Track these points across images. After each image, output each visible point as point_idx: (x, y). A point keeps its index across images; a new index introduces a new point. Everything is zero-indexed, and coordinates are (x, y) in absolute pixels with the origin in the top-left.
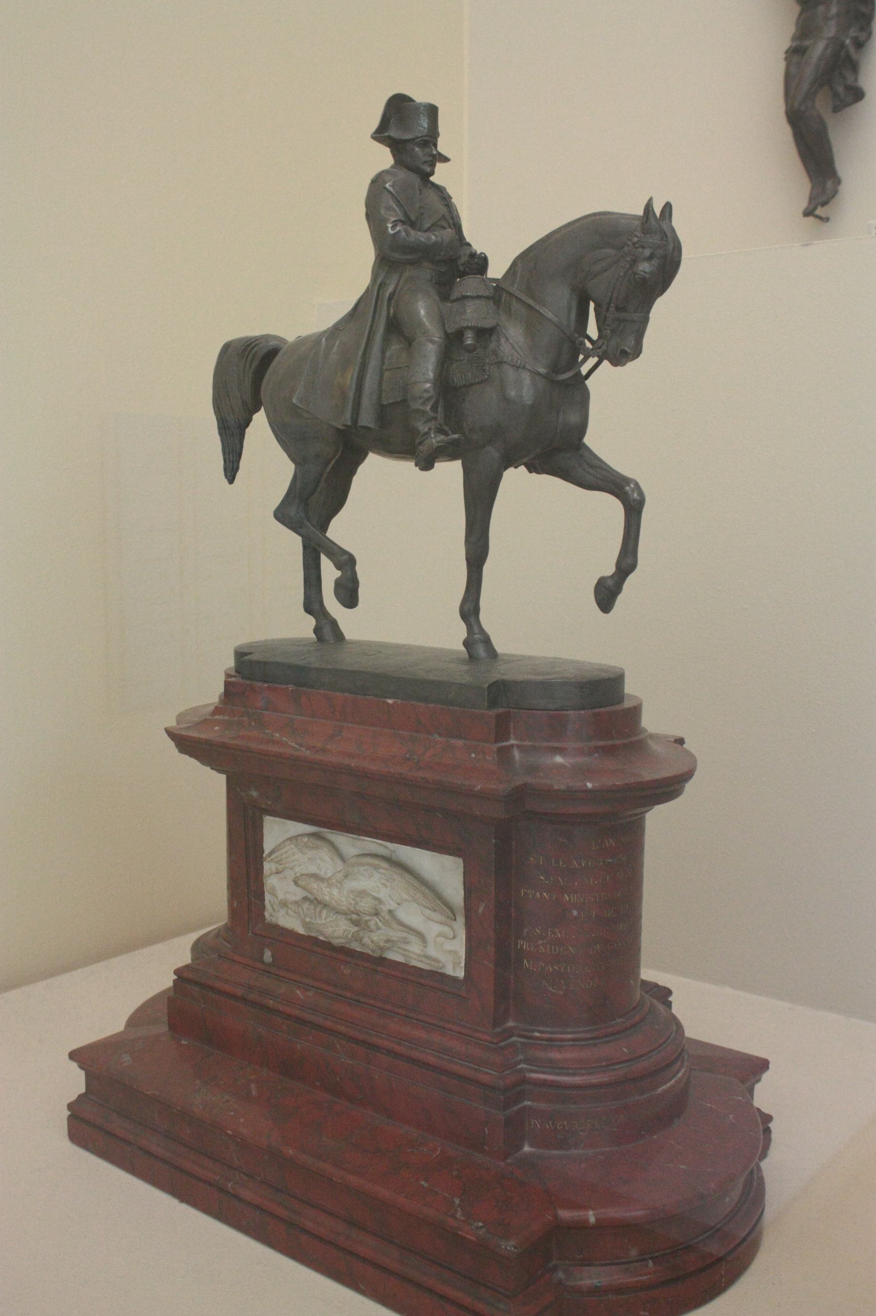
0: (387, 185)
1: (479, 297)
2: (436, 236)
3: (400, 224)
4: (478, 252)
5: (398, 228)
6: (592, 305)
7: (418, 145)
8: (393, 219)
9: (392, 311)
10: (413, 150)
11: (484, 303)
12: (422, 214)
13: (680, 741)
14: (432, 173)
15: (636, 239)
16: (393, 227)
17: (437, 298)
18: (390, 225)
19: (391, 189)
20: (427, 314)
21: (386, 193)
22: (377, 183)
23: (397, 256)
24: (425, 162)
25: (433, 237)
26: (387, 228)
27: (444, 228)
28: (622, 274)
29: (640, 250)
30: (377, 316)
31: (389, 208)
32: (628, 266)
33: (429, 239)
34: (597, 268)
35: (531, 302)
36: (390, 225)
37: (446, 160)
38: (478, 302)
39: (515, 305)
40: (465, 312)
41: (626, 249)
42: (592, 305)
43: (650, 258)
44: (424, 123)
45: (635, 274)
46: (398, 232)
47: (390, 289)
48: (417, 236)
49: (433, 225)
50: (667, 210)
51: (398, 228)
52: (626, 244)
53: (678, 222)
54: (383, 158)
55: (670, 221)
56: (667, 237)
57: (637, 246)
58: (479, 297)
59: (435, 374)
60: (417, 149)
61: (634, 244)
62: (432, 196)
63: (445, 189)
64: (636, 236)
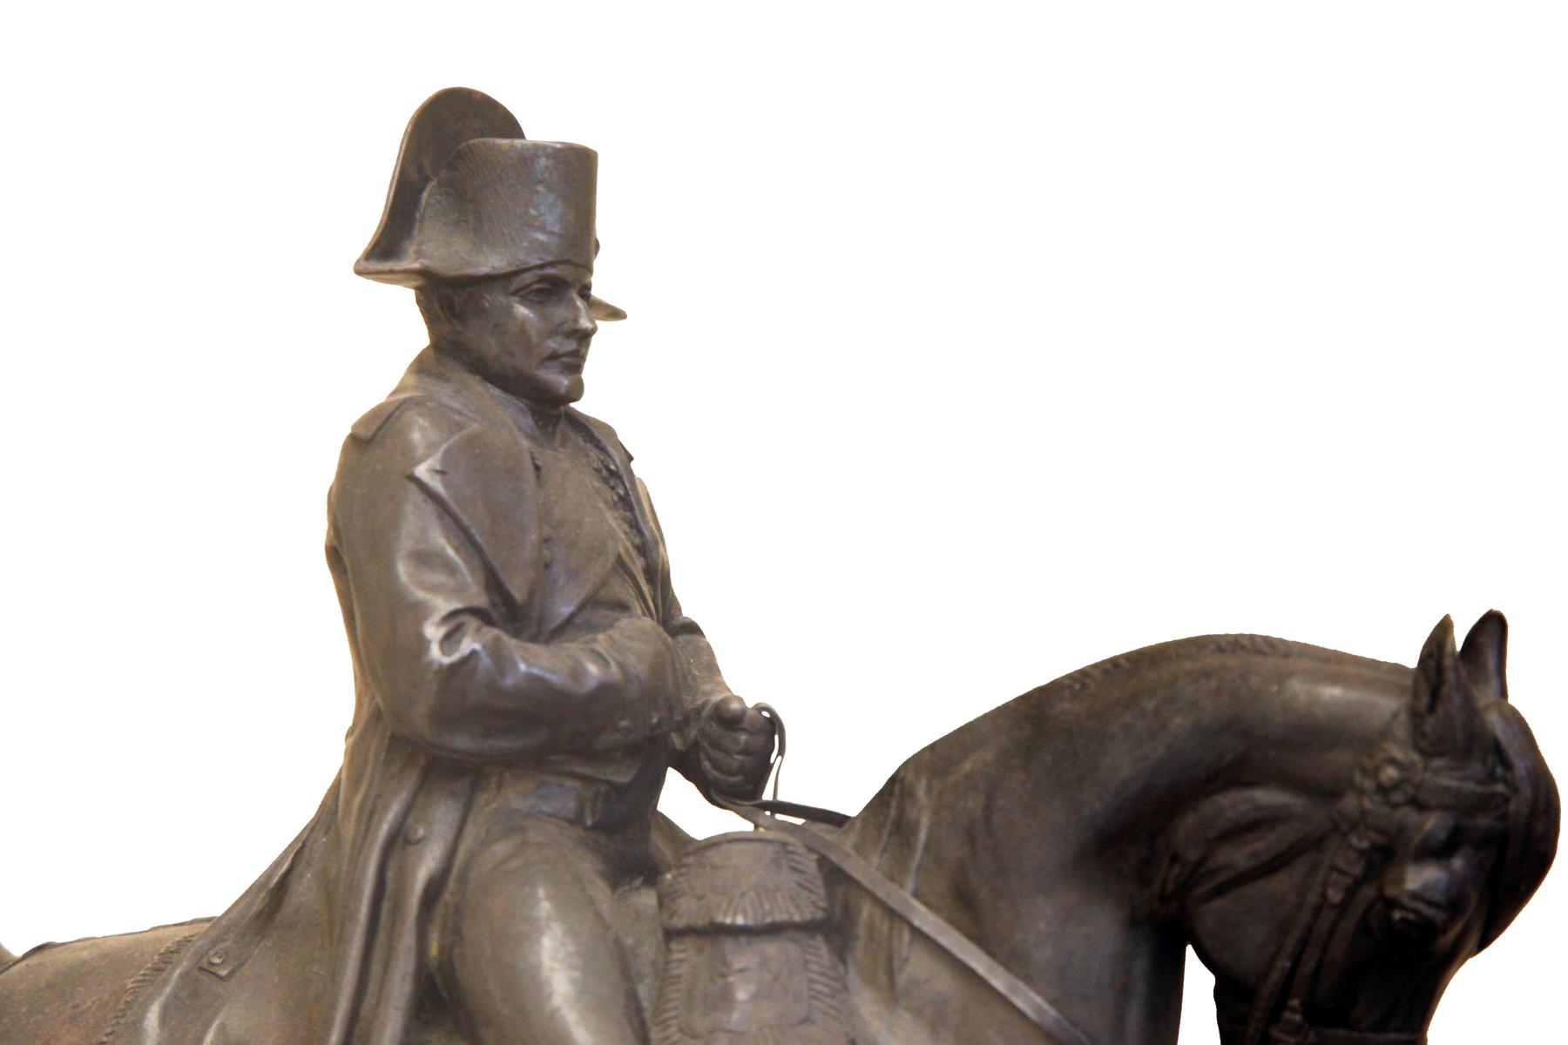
0: (422, 471)
1: (773, 930)
2: (599, 658)
3: (473, 623)
4: (750, 704)
5: (468, 645)
6: (1198, 981)
7: (524, 294)
8: (444, 606)
9: (434, 949)
10: (508, 311)
11: (793, 950)
12: (547, 566)
13: (631, 458)
14: (577, 391)
15: (1391, 773)
16: (449, 640)
17: (588, 865)
18: (433, 632)
19: (436, 484)
20: (581, 990)
21: (413, 487)
22: (371, 442)
23: (462, 742)
24: (554, 356)
25: (593, 669)
26: (423, 643)
27: (623, 607)
28: (1335, 896)
29: (1411, 816)
30: (376, 968)
31: (425, 558)
32: (1357, 870)
33: (577, 673)
34: (1238, 856)
35: (978, 961)
36: (433, 632)
37: (615, 314)
38: (772, 948)
39: (918, 967)
40: (725, 998)
41: (1350, 803)
42: (1198, 981)
43: (1439, 852)
44: (550, 214)
45: (1392, 904)
46: (465, 661)
47: (425, 867)
48: (532, 662)
49: (582, 607)
50: (1487, 640)
51: (468, 645)
52: (1352, 785)
53: (1532, 687)
54: (390, 332)
55: (1503, 693)
56: (1506, 764)
57: (1397, 797)
58: (773, 930)
59: (538, 942)
60: (522, 311)
61: (1383, 790)
62: (570, 473)
63: (610, 432)
64: (1393, 762)
